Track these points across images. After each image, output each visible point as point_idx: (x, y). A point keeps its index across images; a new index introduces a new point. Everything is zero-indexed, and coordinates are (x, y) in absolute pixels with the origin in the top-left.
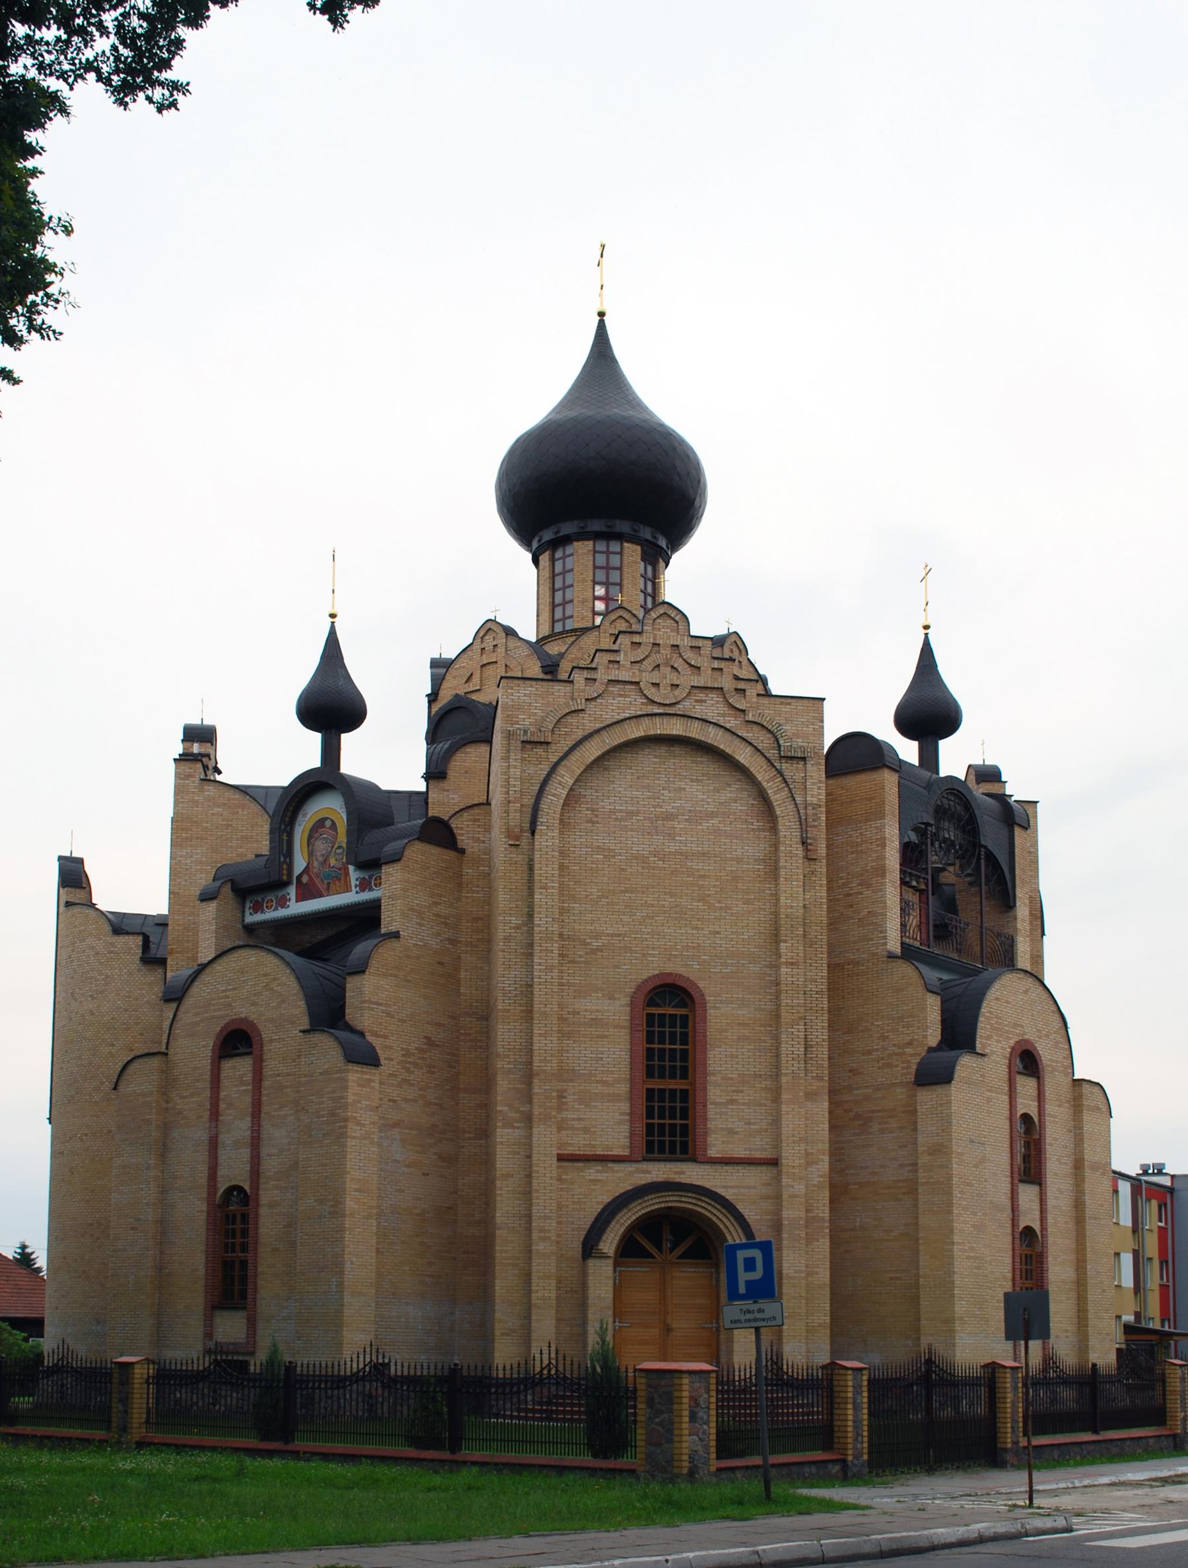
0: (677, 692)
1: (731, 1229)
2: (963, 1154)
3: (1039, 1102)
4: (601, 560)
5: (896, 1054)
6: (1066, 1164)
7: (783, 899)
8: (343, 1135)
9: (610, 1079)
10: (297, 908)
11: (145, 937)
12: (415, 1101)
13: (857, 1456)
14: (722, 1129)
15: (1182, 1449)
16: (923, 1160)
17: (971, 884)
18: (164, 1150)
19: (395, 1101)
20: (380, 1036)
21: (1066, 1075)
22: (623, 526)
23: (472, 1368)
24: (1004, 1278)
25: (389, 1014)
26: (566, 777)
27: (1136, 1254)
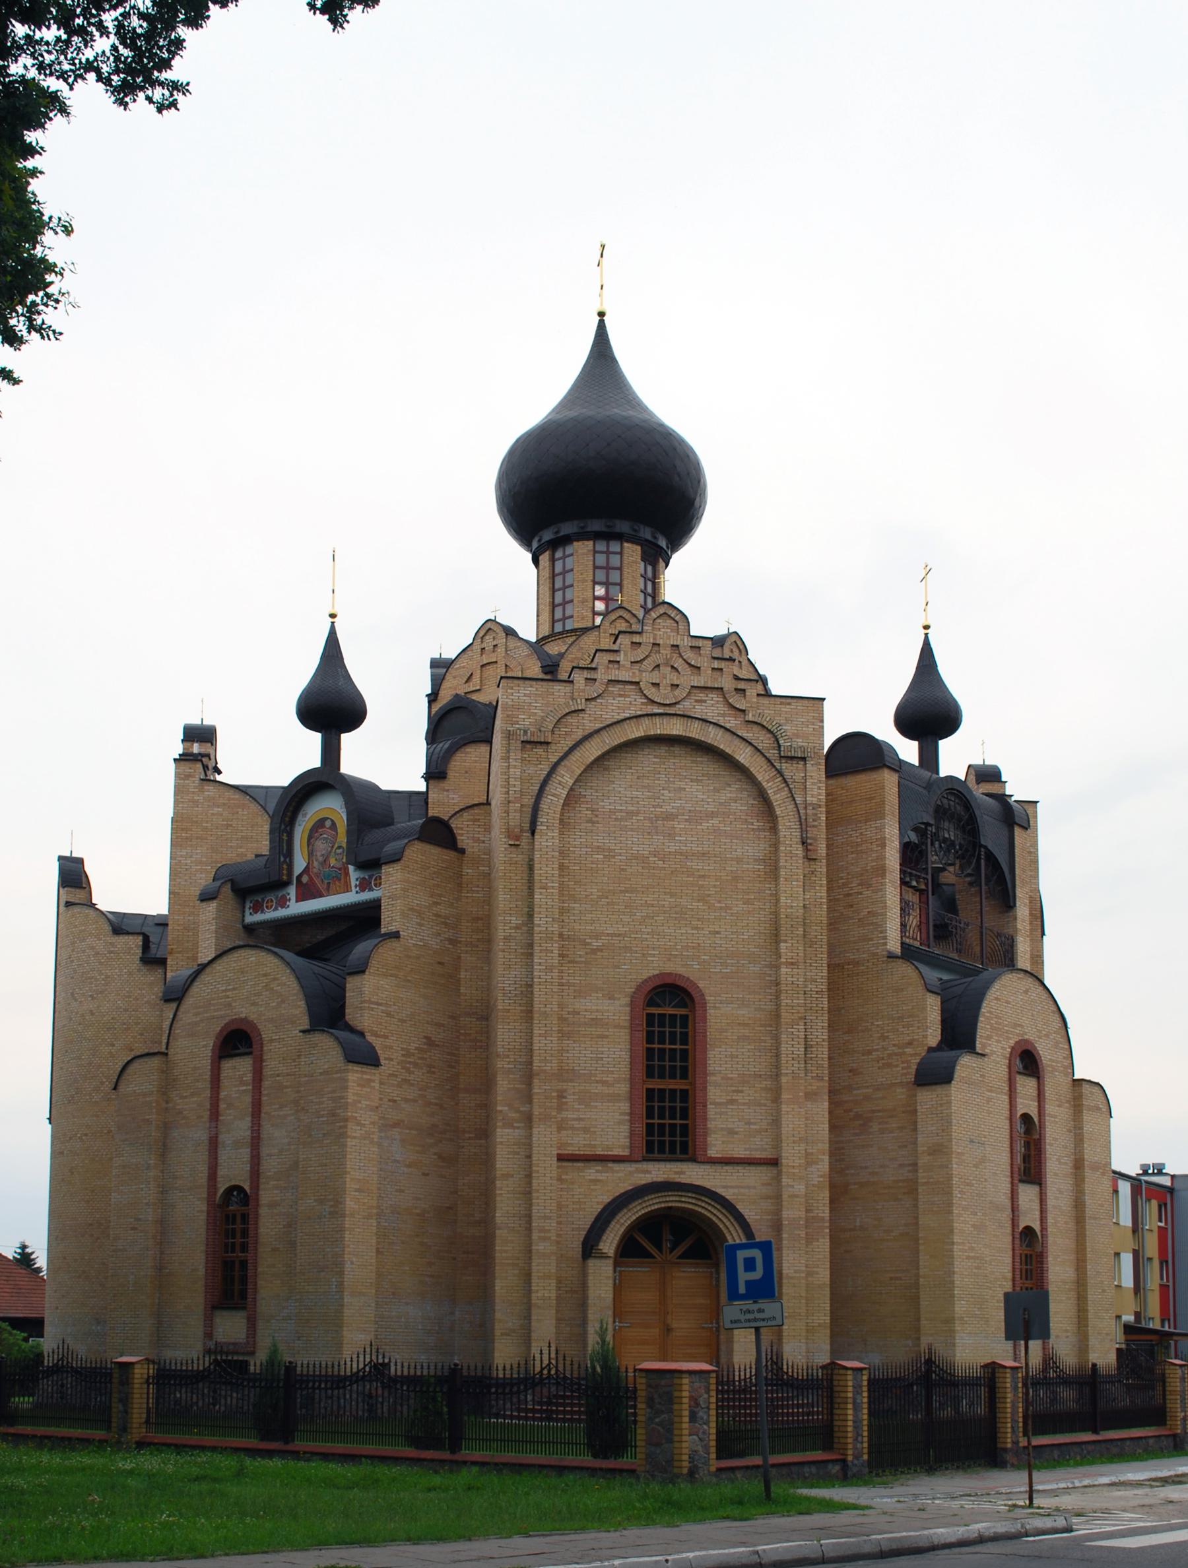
0: (677, 692)
1: (731, 1229)
2: (963, 1154)
3: (1039, 1102)
4: (601, 560)
5: (896, 1054)
6: (1066, 1164)
7: (783, 899)
8: (343, 1135)
9: (610, 1079)
10: (297, 908)
11: (145, 937)
12: (415, 1101)
13: (857, 1456)
14: (722, 1129)
15: (1182, 1449)
16: (923, 1160)
17: (971, 884)
18: (164, 1150)
19: (395, 1101)
20: (380, 1036)
21: (1066, 1075)
22: (623, 526)
23: (472, 1368)
24: (1004, 1278)
25: (389, 1014)
26: (566, 777)
27: (1136, 1254)
